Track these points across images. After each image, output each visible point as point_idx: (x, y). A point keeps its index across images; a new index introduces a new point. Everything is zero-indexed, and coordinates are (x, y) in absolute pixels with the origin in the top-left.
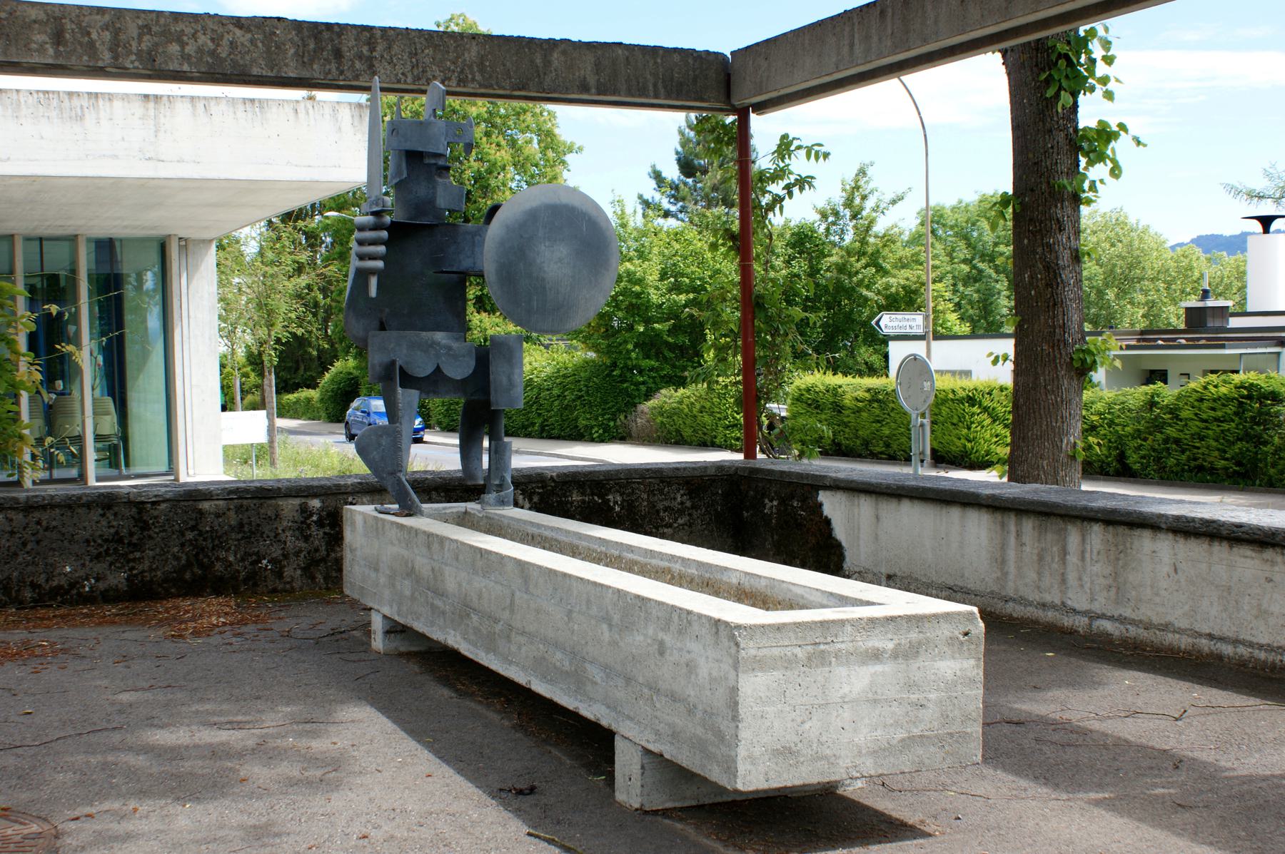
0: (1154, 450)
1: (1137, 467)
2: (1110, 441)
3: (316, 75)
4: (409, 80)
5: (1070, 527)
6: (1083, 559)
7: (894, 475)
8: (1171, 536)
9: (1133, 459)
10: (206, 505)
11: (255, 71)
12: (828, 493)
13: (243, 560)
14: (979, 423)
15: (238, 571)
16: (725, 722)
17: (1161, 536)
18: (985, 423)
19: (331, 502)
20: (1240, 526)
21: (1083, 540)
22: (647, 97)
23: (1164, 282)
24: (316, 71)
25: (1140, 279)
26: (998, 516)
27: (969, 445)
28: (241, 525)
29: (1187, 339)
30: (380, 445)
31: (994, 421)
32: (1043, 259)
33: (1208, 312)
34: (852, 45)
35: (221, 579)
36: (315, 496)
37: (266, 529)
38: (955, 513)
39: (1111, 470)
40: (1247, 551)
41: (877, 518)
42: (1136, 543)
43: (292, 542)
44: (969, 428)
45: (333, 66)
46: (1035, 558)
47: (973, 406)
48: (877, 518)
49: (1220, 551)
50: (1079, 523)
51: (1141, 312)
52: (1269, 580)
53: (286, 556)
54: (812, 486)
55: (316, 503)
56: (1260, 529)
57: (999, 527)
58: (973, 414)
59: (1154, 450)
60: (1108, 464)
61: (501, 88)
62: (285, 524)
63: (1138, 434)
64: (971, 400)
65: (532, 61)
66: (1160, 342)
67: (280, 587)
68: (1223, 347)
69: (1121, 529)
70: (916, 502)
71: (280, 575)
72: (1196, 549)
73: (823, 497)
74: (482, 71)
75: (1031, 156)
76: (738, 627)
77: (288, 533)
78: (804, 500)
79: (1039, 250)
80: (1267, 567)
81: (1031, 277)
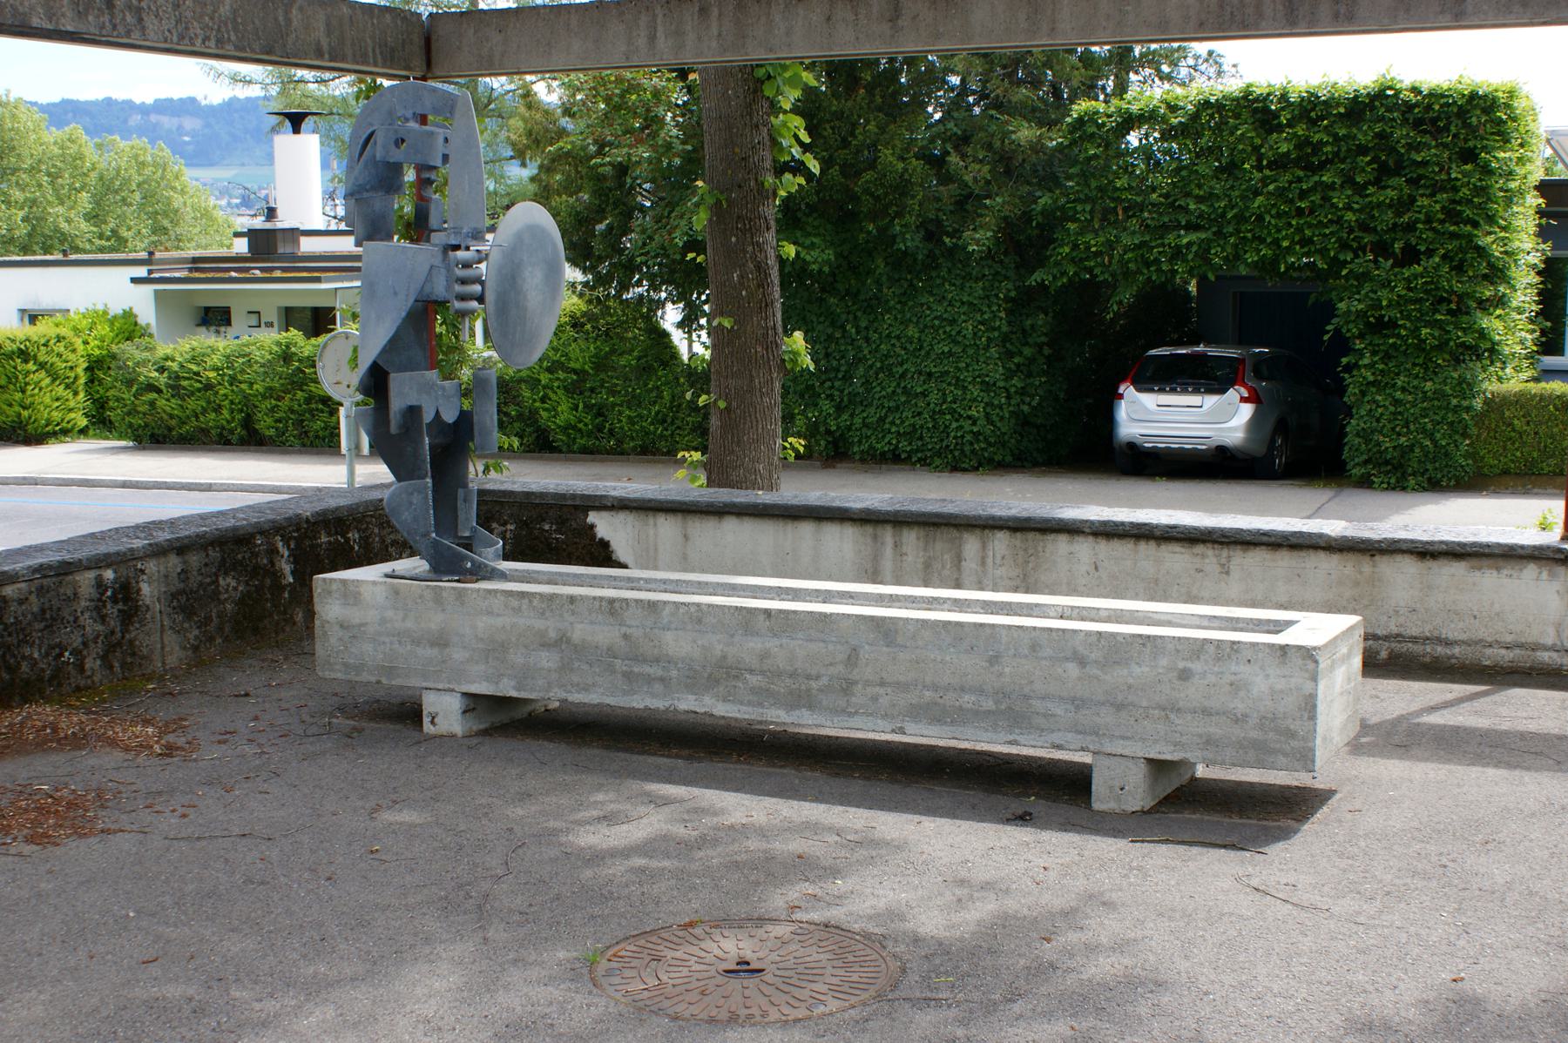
0: (292, 411)
1: (272, 432)
2: (232, 402)
3: (93, 30)
4: (175, 39)
5: (966, 535)
6: (983, 563)
7: (1262, 512)
8: (1091, 539)
9: (265, 424)
10: (9, 591)
11: (36, 22)
12: (604, 514)
13: (47, 654)
14: (37, 384)
15: (43, 670)
16: (1298, 722)
17: (1081, 539)
18: (43, 384)
19: (123, 571)
20: (1174, 527)
21: (984, 547)
22: (368, 64)
23: (49, 174)
24: (91, 25)
25: (15, 171)
26: (869, 529)
27: (25, 413)
28: (43, 611)
29: (262, 269)
30: (411, 503)
31: (54, 380)
32: (754, 258)
33: (279, 236)
34: (652, 38)
35: (27, 682)
36: (108, 566)
37: (65, 613)
38: (806, 529)
39: (234, 438)
40: (1176, 547)
41: (686, 537)
42: (1050, 547)
43: (91, 626)
44: (23, 391)
45: (107, 18)
46: (920, 566)
47: (26, 361)
48: (686, 537)
49: (1146, 549)
50: (978, 531)
51: (21, 214)
52: (1199, 571)
53: (85, 644)
54: (576, 507)
55: (109, 574)
56: (1196, 529)
57: (869, 540)
58: (28, 372)
59: (292, 411)
60: (232, 432)
61: (253, 51)
62: (83, 604)
63: (269, 393)
64: (24, 355)
65: (276, 19)
66: (233, 274)
67: (82, 683)
68: (318, 280)
69: (1031, 535)
70: (746, 519)
71: (81, 668)
72: (1121, 548)
73: (593, 517)
74: (236, 30)
75: (737, 150)
76: (1315, 648)
77: (87, 615)
78: (562, 523)
79: (750, 249)
80: (1197, 560)
81: (741, 277)
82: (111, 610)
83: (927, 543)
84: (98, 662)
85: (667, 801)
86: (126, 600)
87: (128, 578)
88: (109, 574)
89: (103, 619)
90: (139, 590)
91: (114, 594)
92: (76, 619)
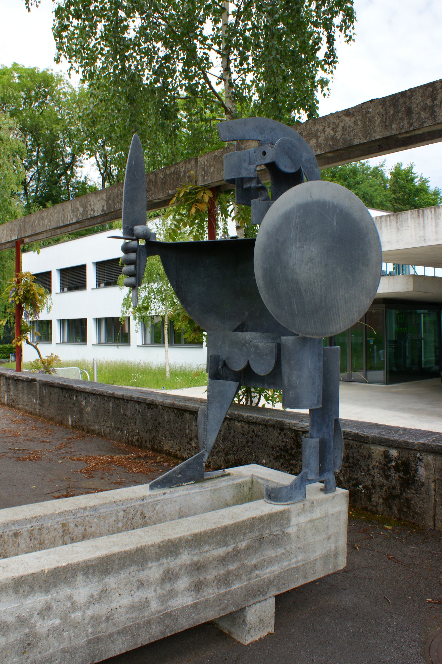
36: (396, 448)
37: (363, 464)
43: (378, 478)
55: (394, 453)
71: (369, 499)
77: (376, 471)
82: (395, 476)
83: (397, 217)
84: (381, 500)
85: (158, 199)
86: (406, 472)
87: (408, 460)
88: (394, 453)
89: (387, 477)
90: (416, 471)
91: (397, 464)
92: (369, 470)
